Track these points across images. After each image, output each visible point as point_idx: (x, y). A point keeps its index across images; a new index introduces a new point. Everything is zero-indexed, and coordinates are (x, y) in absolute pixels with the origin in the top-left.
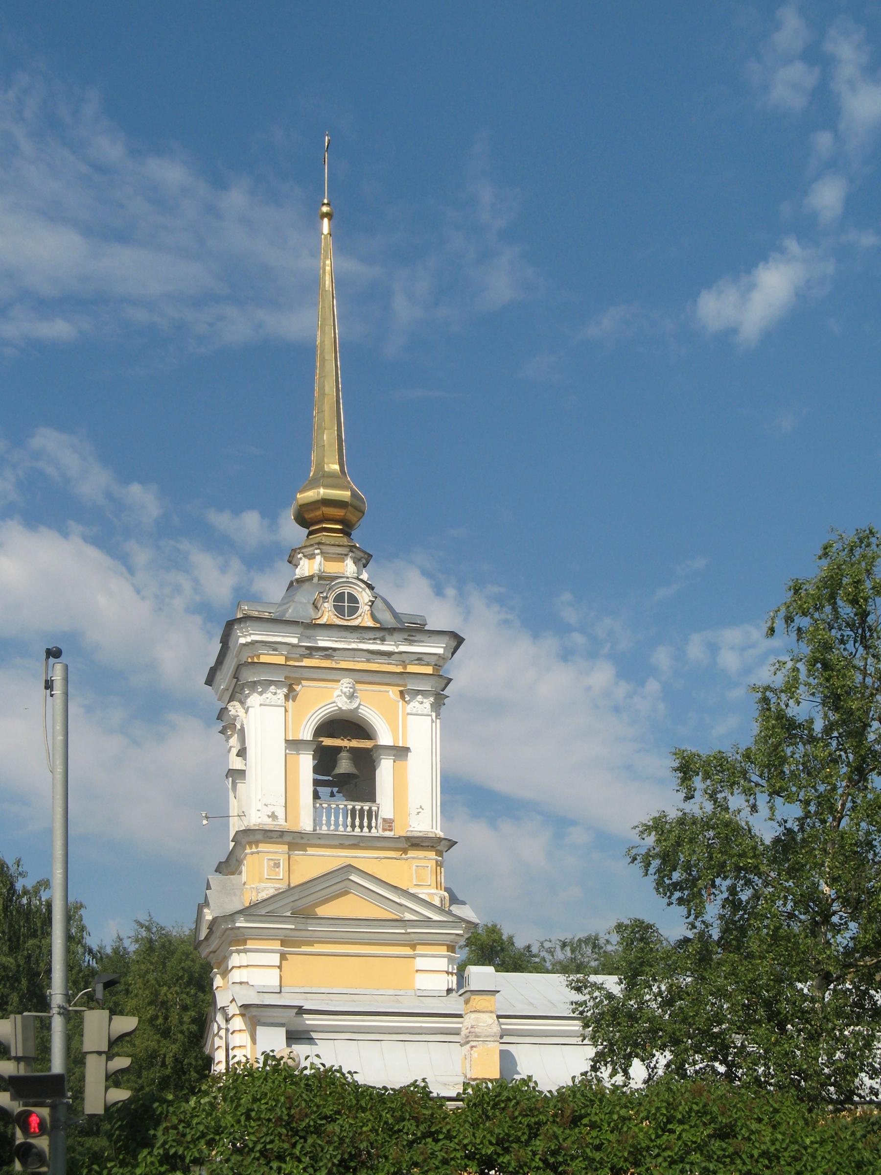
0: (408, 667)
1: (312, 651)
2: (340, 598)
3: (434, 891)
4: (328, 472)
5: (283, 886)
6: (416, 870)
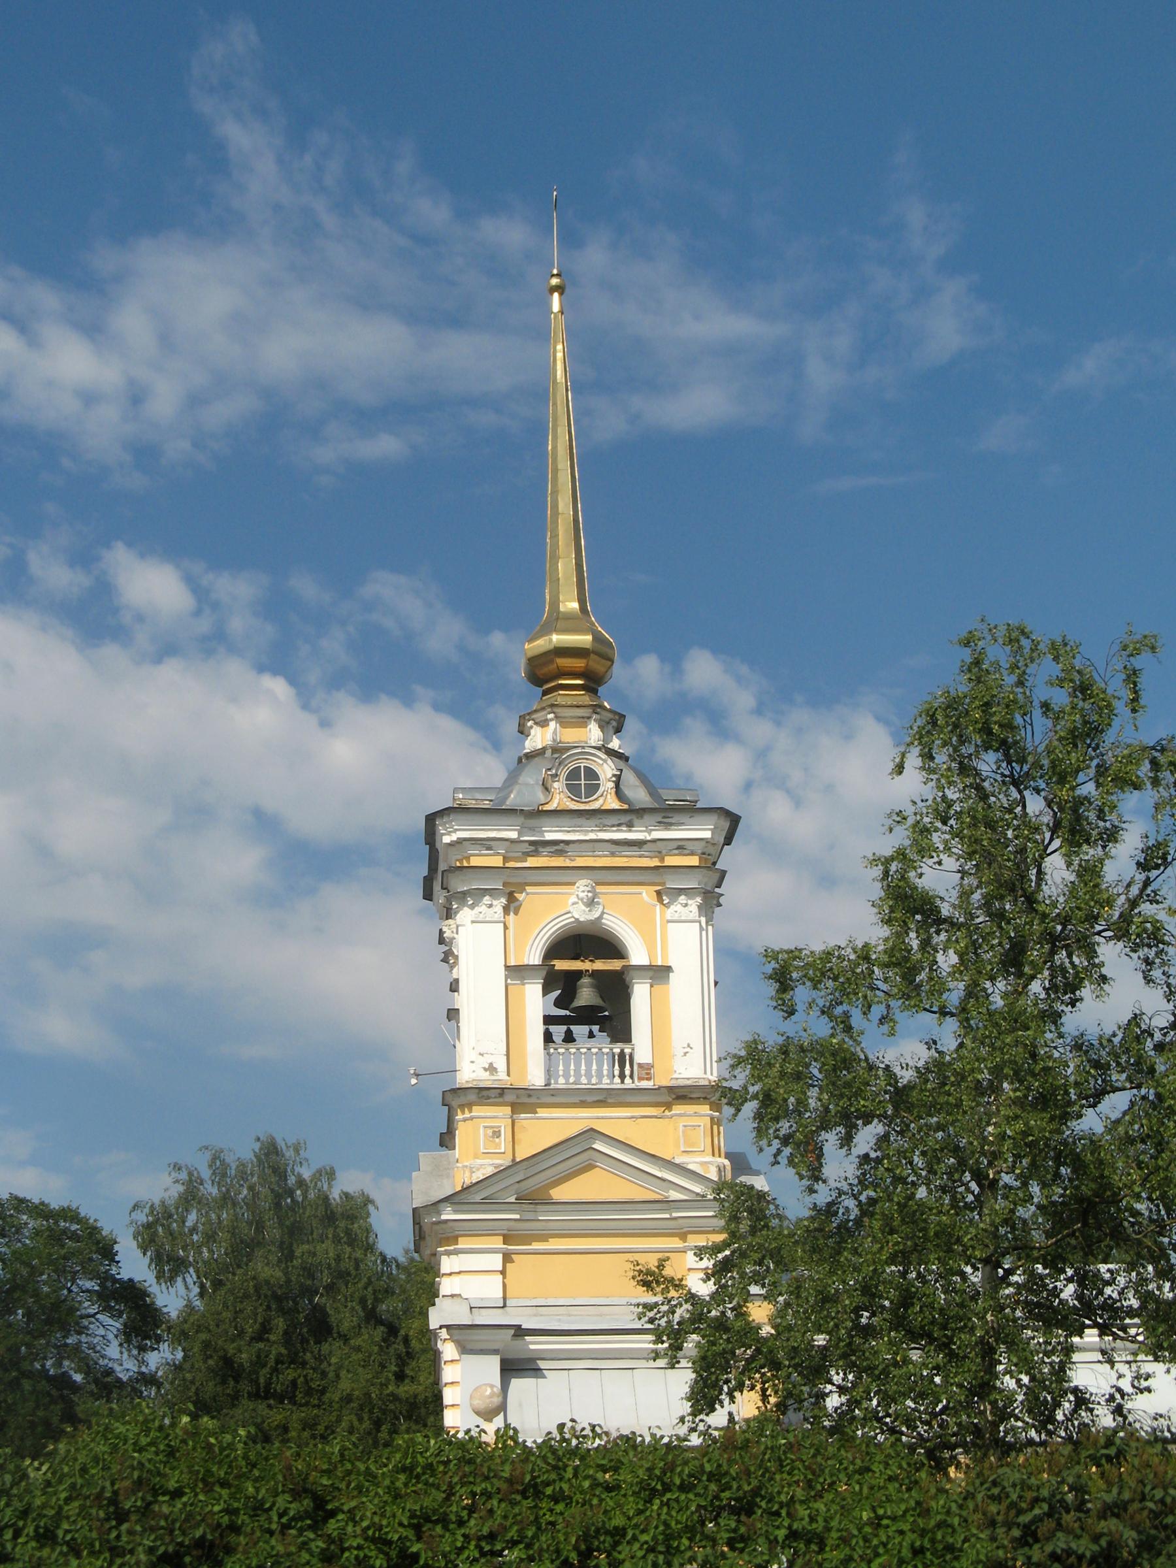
0: (667, 858)
1: (537, 847)
2: (574, 774)
3: (709, 1158)
4: (564, 613)
5: (505, 1161)
6: (683, 1132)
